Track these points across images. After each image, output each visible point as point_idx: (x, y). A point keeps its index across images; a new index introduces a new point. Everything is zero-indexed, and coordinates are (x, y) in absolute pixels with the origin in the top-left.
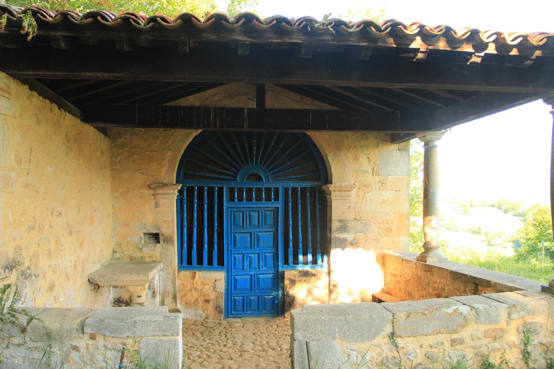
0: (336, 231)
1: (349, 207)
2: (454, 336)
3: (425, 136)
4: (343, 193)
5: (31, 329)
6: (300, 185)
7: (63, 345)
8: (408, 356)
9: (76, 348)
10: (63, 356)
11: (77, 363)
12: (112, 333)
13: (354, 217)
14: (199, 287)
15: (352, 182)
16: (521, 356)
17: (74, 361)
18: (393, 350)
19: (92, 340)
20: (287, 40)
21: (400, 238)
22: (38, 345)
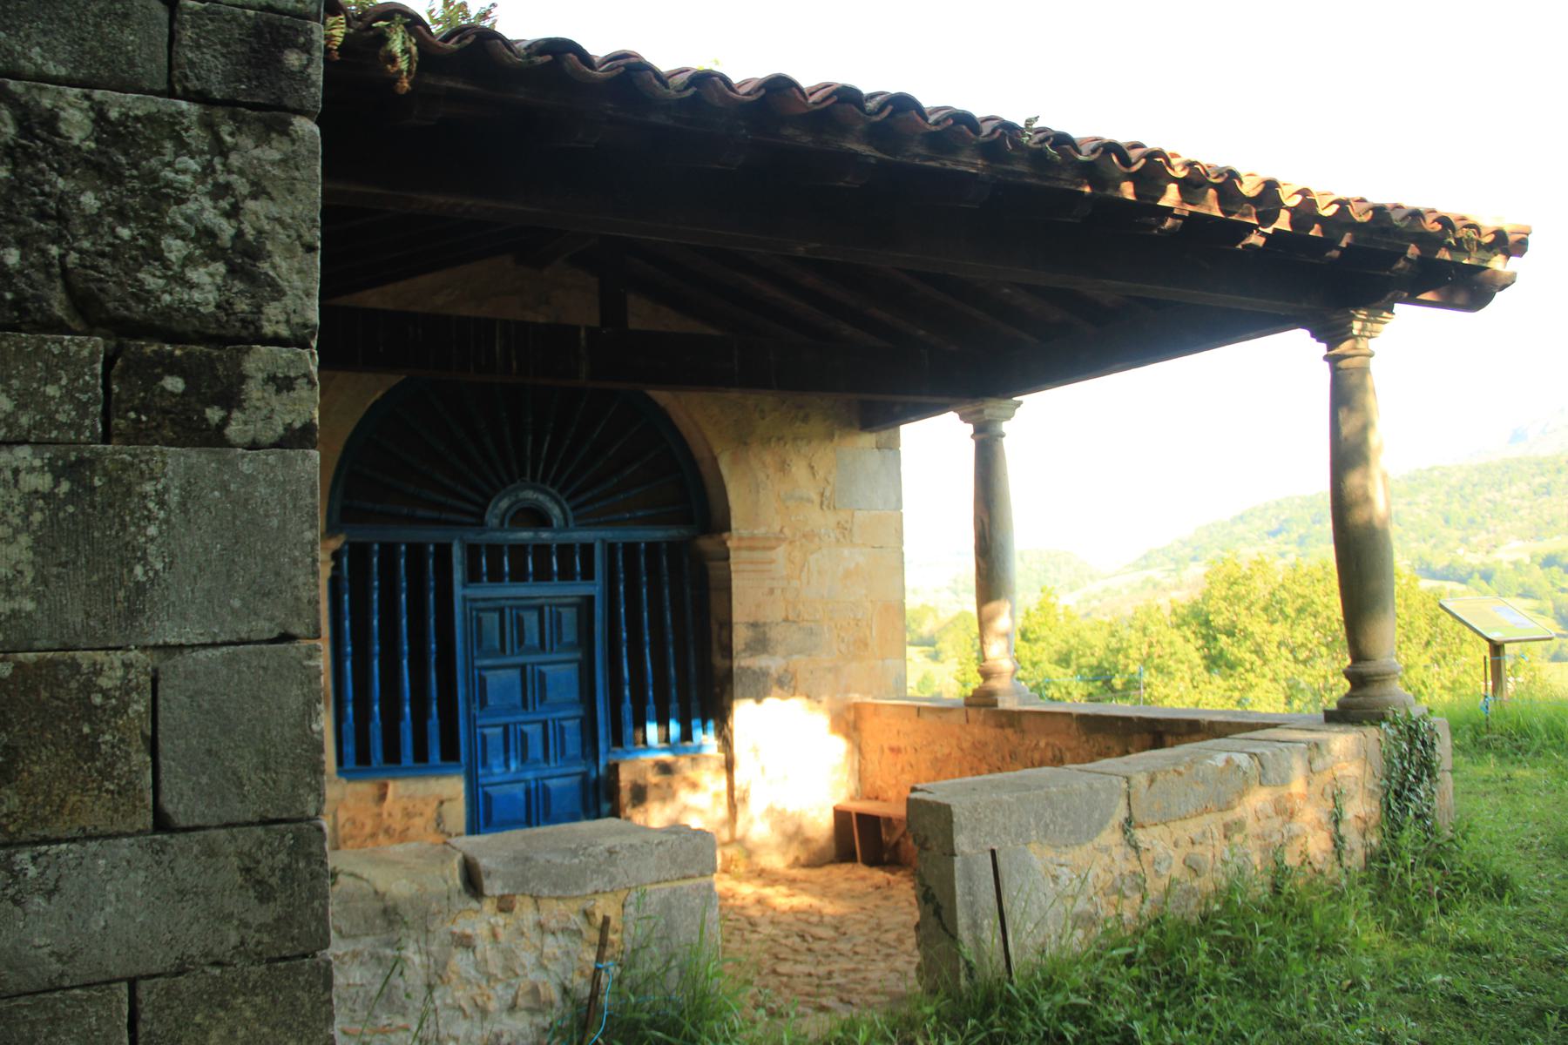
0: (744, 650)
1: (772, 591)
2: (1229, 816)
3: (981, 411)
4: (758, 555)
5: (339, 904)
6: (642, 535)
7: (431, 936)
8: (1156, 867)
9: (465, 942)
10: (429, 966)
11: (469, 982)
12: (555, 886)
13: (783, 615)
15: (777, 529)
16: (1331, 845)
17: (460, 977)
18: (1130, 857)
19: (503, 915)
20: (950, 165)
22: (360, 947)
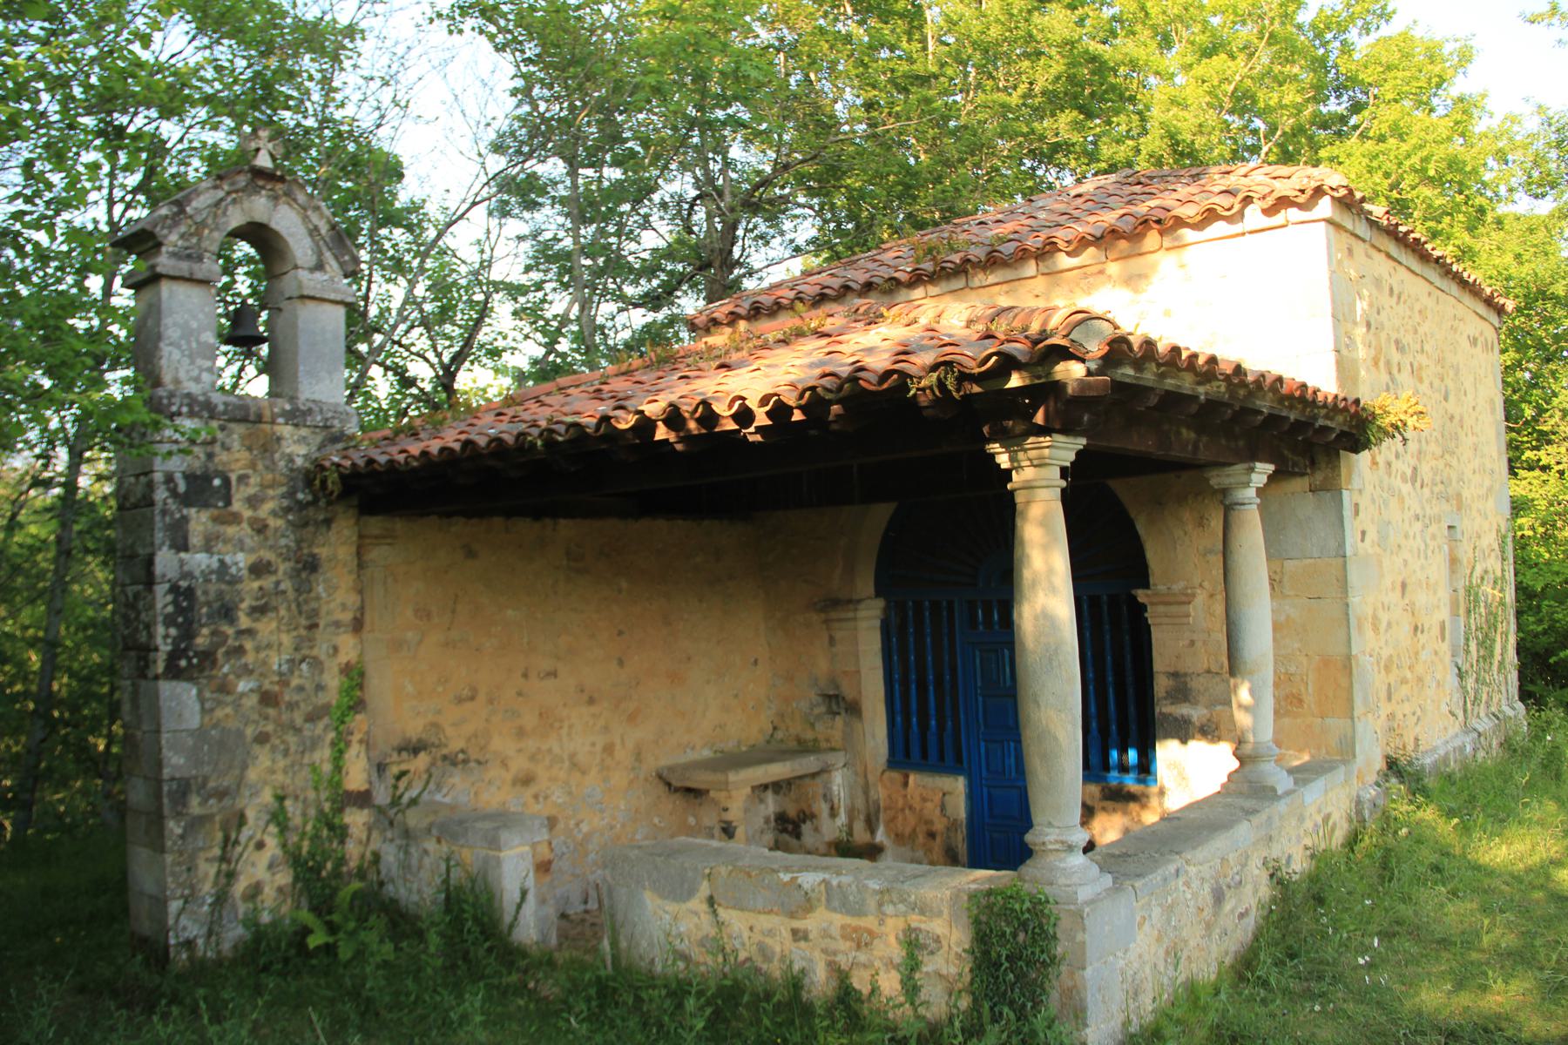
1: (1192, 643)
2: (797, 924)
4: (1174, 609)
14: (917, 804)
21: (1328, 721)
